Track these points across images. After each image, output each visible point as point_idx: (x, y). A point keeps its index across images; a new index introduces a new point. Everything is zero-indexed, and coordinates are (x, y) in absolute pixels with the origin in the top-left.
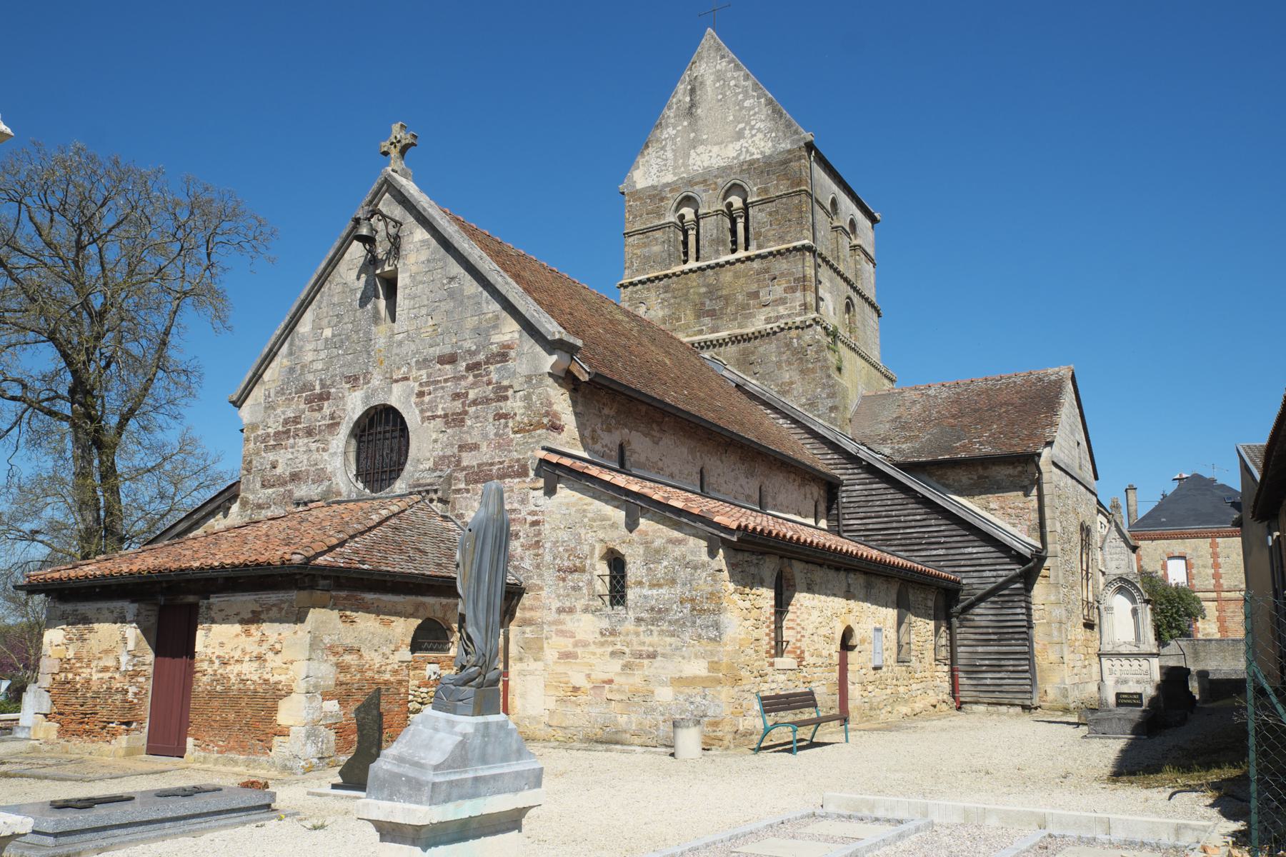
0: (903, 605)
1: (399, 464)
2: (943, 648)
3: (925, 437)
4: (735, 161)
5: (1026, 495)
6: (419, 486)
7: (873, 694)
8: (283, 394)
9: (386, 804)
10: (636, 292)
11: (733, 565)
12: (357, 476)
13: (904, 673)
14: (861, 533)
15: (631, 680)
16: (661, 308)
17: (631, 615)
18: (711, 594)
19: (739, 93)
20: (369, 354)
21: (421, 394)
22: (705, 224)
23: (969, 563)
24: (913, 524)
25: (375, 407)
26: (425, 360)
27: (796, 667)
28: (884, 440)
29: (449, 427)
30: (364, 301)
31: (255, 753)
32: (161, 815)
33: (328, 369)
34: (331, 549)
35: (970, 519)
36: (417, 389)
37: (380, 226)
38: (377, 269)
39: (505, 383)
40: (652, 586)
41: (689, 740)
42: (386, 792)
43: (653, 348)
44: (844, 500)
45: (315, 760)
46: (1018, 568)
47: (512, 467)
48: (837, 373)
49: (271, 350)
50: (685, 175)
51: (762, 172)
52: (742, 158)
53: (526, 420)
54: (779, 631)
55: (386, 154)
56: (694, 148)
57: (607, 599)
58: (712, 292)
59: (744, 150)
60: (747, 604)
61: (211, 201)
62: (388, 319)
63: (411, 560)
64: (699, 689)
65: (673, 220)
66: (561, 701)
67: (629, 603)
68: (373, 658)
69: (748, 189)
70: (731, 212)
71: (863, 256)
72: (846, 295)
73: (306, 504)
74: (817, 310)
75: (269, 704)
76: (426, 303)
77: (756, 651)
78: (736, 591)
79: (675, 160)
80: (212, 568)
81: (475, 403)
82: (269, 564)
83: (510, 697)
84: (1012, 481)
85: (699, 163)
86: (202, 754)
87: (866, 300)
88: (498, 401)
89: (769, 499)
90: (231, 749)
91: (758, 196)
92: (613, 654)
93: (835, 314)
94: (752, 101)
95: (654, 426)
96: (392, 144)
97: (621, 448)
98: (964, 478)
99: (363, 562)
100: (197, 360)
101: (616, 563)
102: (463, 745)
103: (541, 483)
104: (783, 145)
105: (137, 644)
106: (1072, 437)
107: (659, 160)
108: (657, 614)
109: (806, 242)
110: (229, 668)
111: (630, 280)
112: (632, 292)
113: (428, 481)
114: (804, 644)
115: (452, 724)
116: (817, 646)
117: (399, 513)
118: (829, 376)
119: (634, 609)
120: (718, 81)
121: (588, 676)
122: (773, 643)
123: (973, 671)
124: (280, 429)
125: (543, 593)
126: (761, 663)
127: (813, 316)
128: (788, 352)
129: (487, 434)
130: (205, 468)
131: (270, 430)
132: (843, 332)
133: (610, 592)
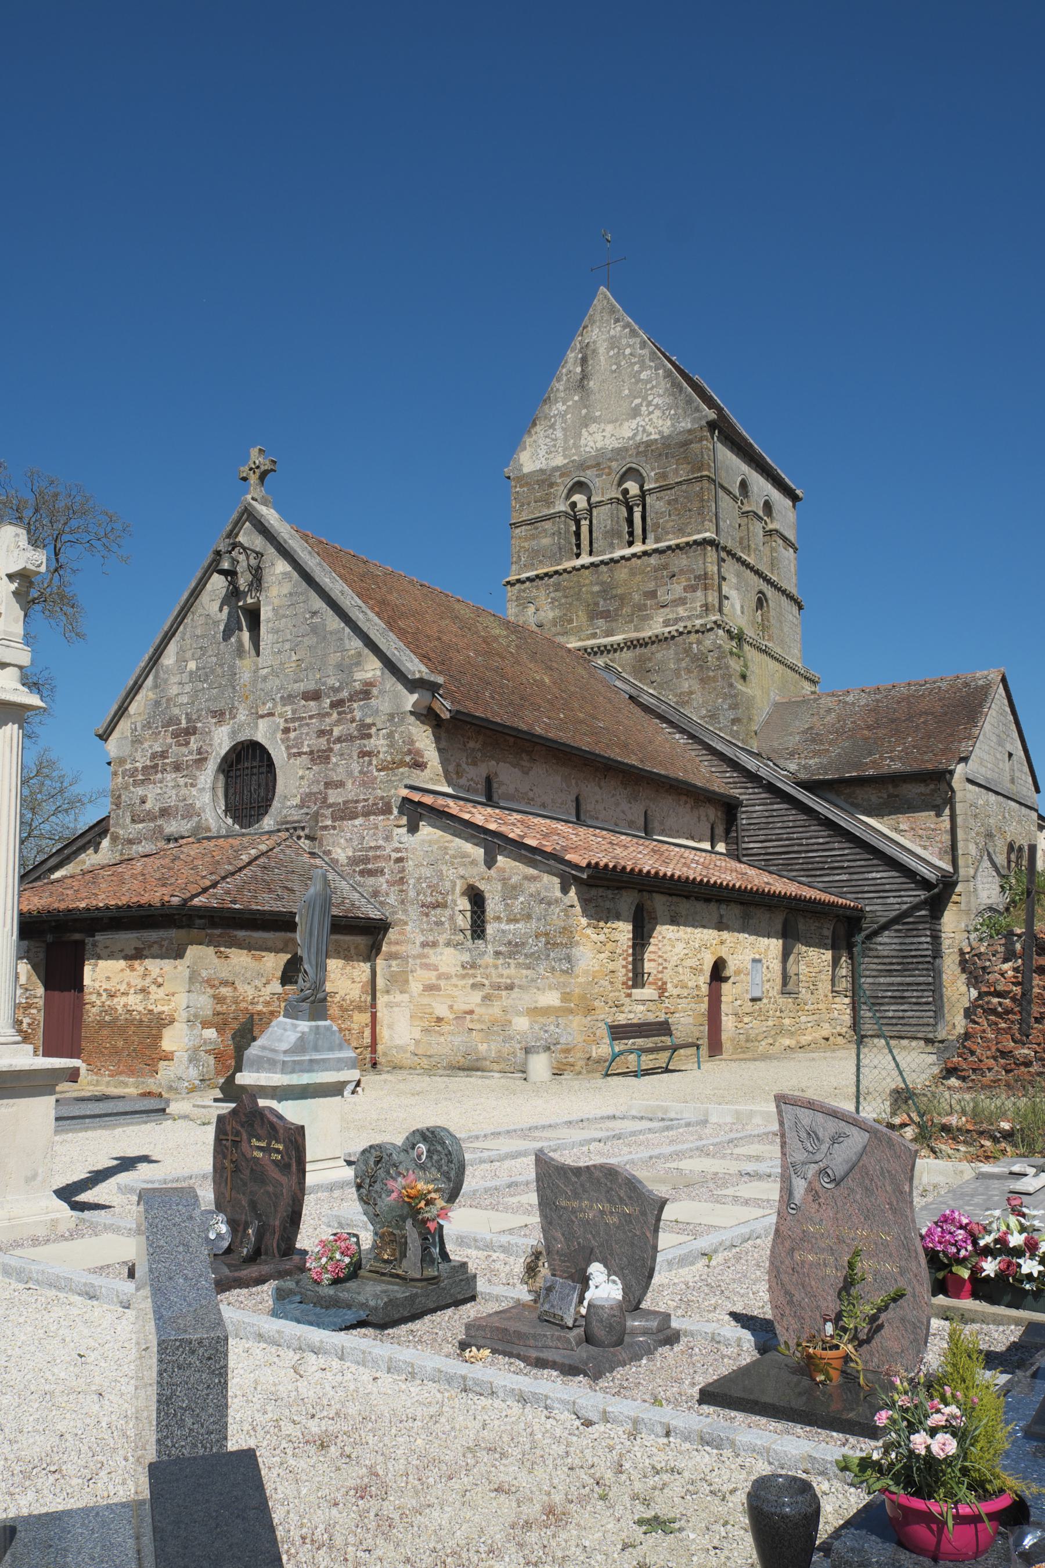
0: (790, 936)
1: (267, 800)
2: (844, 979)
3: (835, 751)
4: (631, 442)
5: (939, 815)
6: (287, 823)
7: (751, 1025)
8: (150, 728)
9: (255, 1075)
10: (524, 591)
11: (585, 900)
12: (226, 811)
13: (791, 1005)
14: (762, 857)
15: (490, 1011)
16: (552, 609)
17: (490, 949)
18: (564, 928)
19: (635, 363)
20: (234, 688)
21: (287, 730)
22: (598, 514)
23: (872, 888)
24: (816, 847)
25: (242, 743)
26: (290, 696)
27: (657, 998)
28: (792, 754)
29: (315, 764)
30: (227, 634)
31: (143, 1075)
32: (82, 1113)
33: (193, 703)
34: (205, 890)
35: (874, 842)
36: (282, 725)
37: (242, 558)
38: (239, 601)
39: (369, 721)
40: (510, 921)
41: (540, 1065)
42: (255, 1067)
43: (531, 666)
44: (744, 822)
45: (197, 1082)
46: (923, 895)
47: (376, 804)
48: (741, 681)
49: (136, 683)
50: (575, 458)
51: (660, 455)
52: (638, 438)
53: (389, 758)
54: (639, 964)
55: (245, 479)
56: (586, 426)
57: (468, 933)
58: (606, 591)
59: (640, 429)
60: (602, 937)
61: (56, 495)
62: (253, 652)
63: (280, 898)
64: (552, 1019)
65: (563, 509)
66: (426, 1031)
67: (488, 937)
68: (247, 991)
69: (645, 474)
70: (626, 499)
71: (780, 542)
72: (757, 589)
73: (176, 840)
74: (720, 610)
75: (154, 1032)
76: (289, 637)
77: (611, 983)
78: (589, 925)
79: (566, 441)
80: (97, 909)
81: (339, 740)
82: (150, 905)
83: (378, 1028)
84: (924, 800)
85: (592, 444)
86: (95, 1078)
87: (784, 592)
88: (362, 738)
89: (656, 824)
90: (121, 1073)
91: (656, 482)
92: (474, 986)
93: (742, 613)
94: (649, 373)
95: (524, 755)
96: (251, 469)
97: (489, 781)
98: (873, 796)
99: (234, 902)
100: (48, 671)
101: (476, 898)
102: (302, 1038)
103: (404, 820)
104: (683, 424)
105: (29, 979)
106: (1000, 749)
107: (548, 440)
108: (514, 948)
109: (707, 535)
110: (116, 1000)
111: (518, 577)
112: (519, 591)
113: (296, 818)
114: (667, 976)
115: (295, 1026)
116: (682, 978)
117: (267, 852)
118: (731, 685)
119: (493, 943)
120: (612, 349)
121: (451, 1007)
122: (631, 975)
123: (876, 1003)
124: (148, 763)
125: (408, 928)
126: (617, 994)
127: (714, 618)
128: (687, 659)
129: (351, 772)
130: (61, 791)
131: (138, 764)
132: (750, 632)
133: (472, 926)
